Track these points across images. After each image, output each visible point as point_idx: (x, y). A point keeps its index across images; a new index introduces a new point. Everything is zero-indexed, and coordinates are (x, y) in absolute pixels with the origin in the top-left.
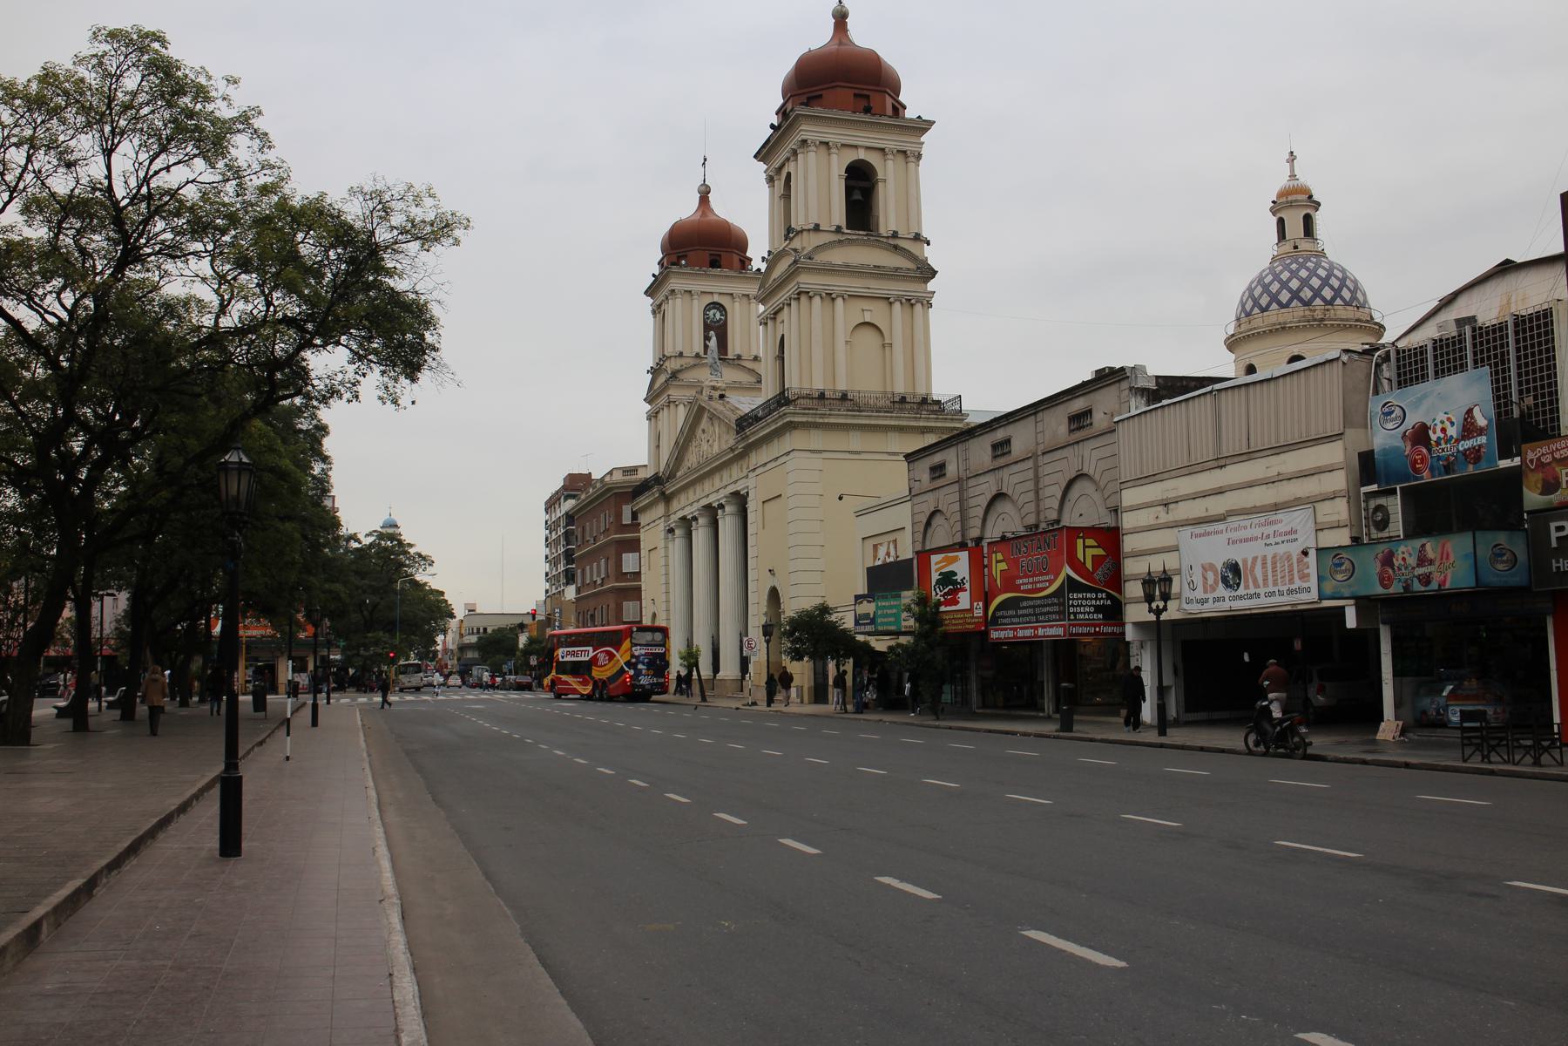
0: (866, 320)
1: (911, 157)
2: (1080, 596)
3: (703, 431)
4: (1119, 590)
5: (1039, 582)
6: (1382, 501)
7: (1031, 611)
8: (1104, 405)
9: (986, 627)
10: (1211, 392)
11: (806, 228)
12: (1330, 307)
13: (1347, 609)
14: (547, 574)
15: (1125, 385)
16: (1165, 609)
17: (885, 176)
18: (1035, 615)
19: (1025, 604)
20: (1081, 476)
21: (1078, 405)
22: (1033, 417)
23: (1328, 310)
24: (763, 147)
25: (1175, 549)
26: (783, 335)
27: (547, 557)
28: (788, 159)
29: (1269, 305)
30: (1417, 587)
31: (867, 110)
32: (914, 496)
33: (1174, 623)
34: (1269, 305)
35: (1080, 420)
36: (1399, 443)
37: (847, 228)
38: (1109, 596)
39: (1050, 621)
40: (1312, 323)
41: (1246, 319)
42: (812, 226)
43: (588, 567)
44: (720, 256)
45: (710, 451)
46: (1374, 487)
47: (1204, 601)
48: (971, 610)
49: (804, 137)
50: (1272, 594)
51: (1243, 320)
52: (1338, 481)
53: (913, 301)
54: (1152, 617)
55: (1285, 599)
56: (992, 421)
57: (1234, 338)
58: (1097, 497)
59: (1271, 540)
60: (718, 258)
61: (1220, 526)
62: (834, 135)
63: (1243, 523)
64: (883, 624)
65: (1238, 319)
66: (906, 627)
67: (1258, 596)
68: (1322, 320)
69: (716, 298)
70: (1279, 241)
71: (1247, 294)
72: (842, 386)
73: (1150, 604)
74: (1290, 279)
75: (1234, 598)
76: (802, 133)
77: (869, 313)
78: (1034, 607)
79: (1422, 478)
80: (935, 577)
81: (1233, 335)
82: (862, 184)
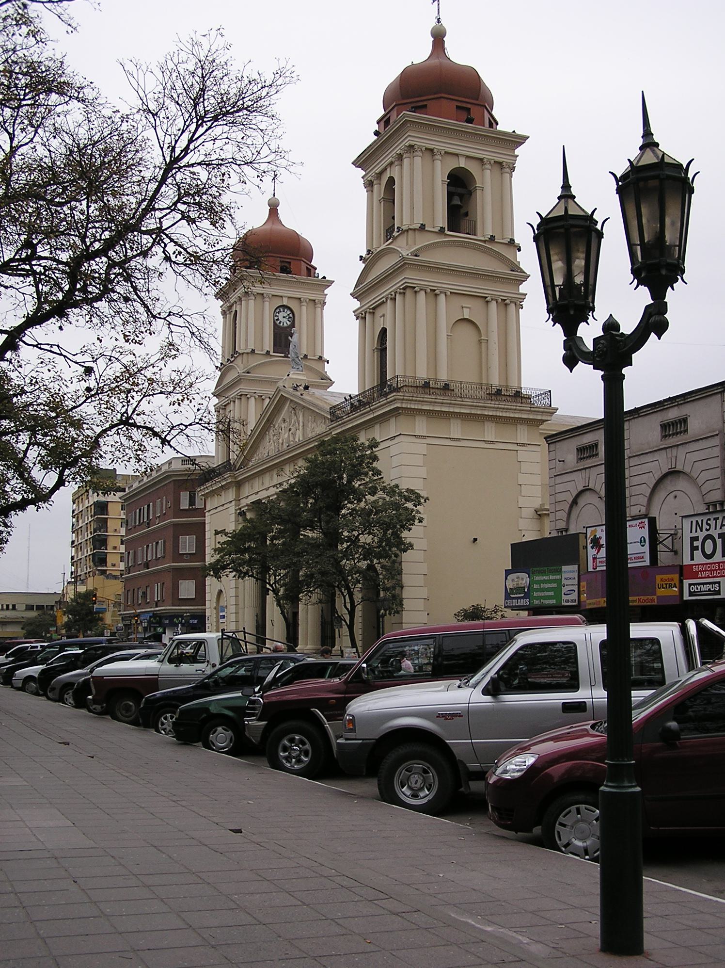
0: (465, 317)
1: (506, 168)
3: (284, 421)
11: (246, 351)
17: (483, 184)
20: (673, 473)
24: (368, 147)
26: (384, 331)
28: (391, 164)
31: (470, 121)
37: (274, 352)
42: (417, 226)
44: (289, 263)
45: (291, 439)
49: (413, 143)
53: (507, 301)
60: (287, 265)
62: (440, 144)
66: (567, 601)
69: (285, 302)
76: (409, 138)
77: (468, 309)
82: (460, 190)
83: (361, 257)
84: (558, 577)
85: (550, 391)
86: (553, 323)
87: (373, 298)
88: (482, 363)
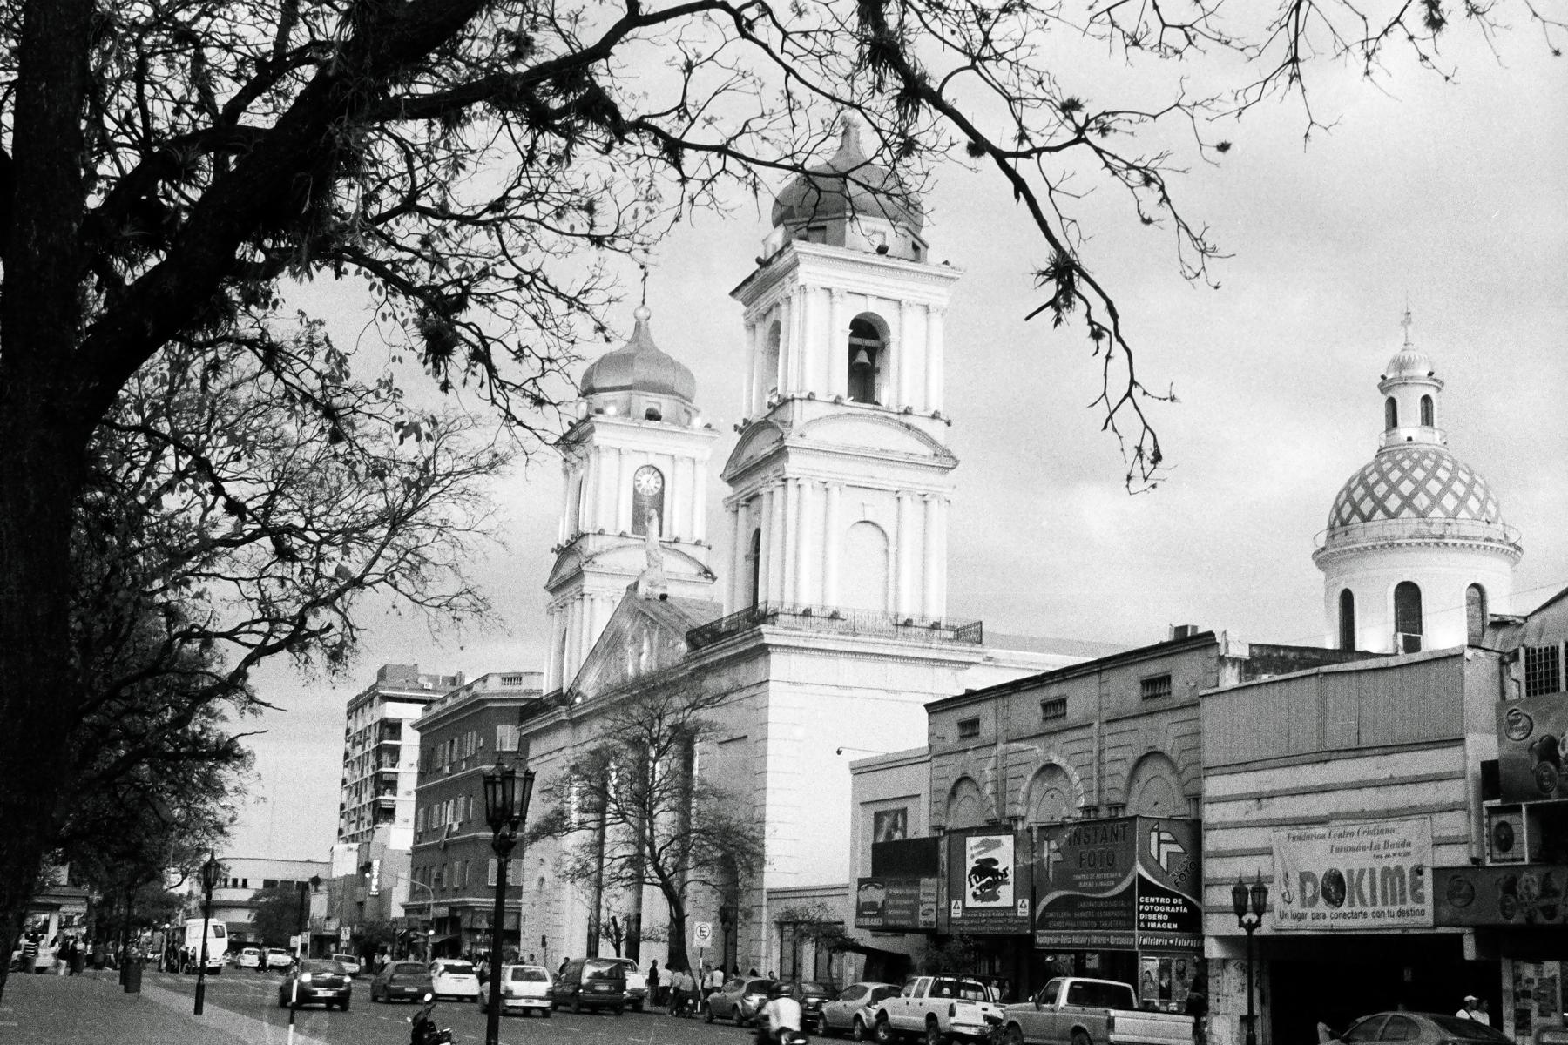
2: (1152, 900)
4: (1199, 897)
5: (1104, 880)
6: (1506, 818)
7: (1090, 914)
8: (1186, 672)
9: (1033, 930)
10: (1317, 674)
12: (1452, 521)
13: (1466, 938)
14: (342, 806)
15: (1212, 652)
16: (1258, 924)
18: (1094, 919)
19: (1083, 905)
21: (1153, 669)
22: (1096, 676)
23: (1449, 524)
25: (1269, 852)
27: (344, 782)
29: (1373, 512)
30: (1541, 919)
32: (936, 756)
33: (1264, 939)
34: (1373, 512)
35: (1156, 685)
36: (1525, 755)
38: (1186, 903)
39: (1067, 928)
40: (1427, 540)
41: (1342, 529)
42: (805, 395)
43: (437, 806)
46: (1497, 802)
47: (1299, 917)
48: (1014, 908)
50: (1380, 914)
51: (1337, 531)
52: (1456, 792)
54: (1243, 932)
55: (1395, 921)
56: (1044, 675)
57: (1325, 553)
58: (1172, 779)
59: (1383, 853)
61: (1320, 830)
63: (1350, 829)
64: (893, 917)
65: (1331, 528)
66: (925, 923)
67: (1365, 915)
68: (1442, 537)
69: (653, 460)
70: (1388, 430)
71: (1344, 495)
72: (833, 604)
73: (1240, 917)
74: (1400, 481)
75: (1337, 916)
78: (1096, 909)
79: (1549, 797)
80: (971, 864)
81: (1323, 549)
82: (868, 342)
83: (736, 426)
84: (915, 892)
85: (981, 623)
86: (226, 948)
87: (747, 486)
88: (891, 583)
